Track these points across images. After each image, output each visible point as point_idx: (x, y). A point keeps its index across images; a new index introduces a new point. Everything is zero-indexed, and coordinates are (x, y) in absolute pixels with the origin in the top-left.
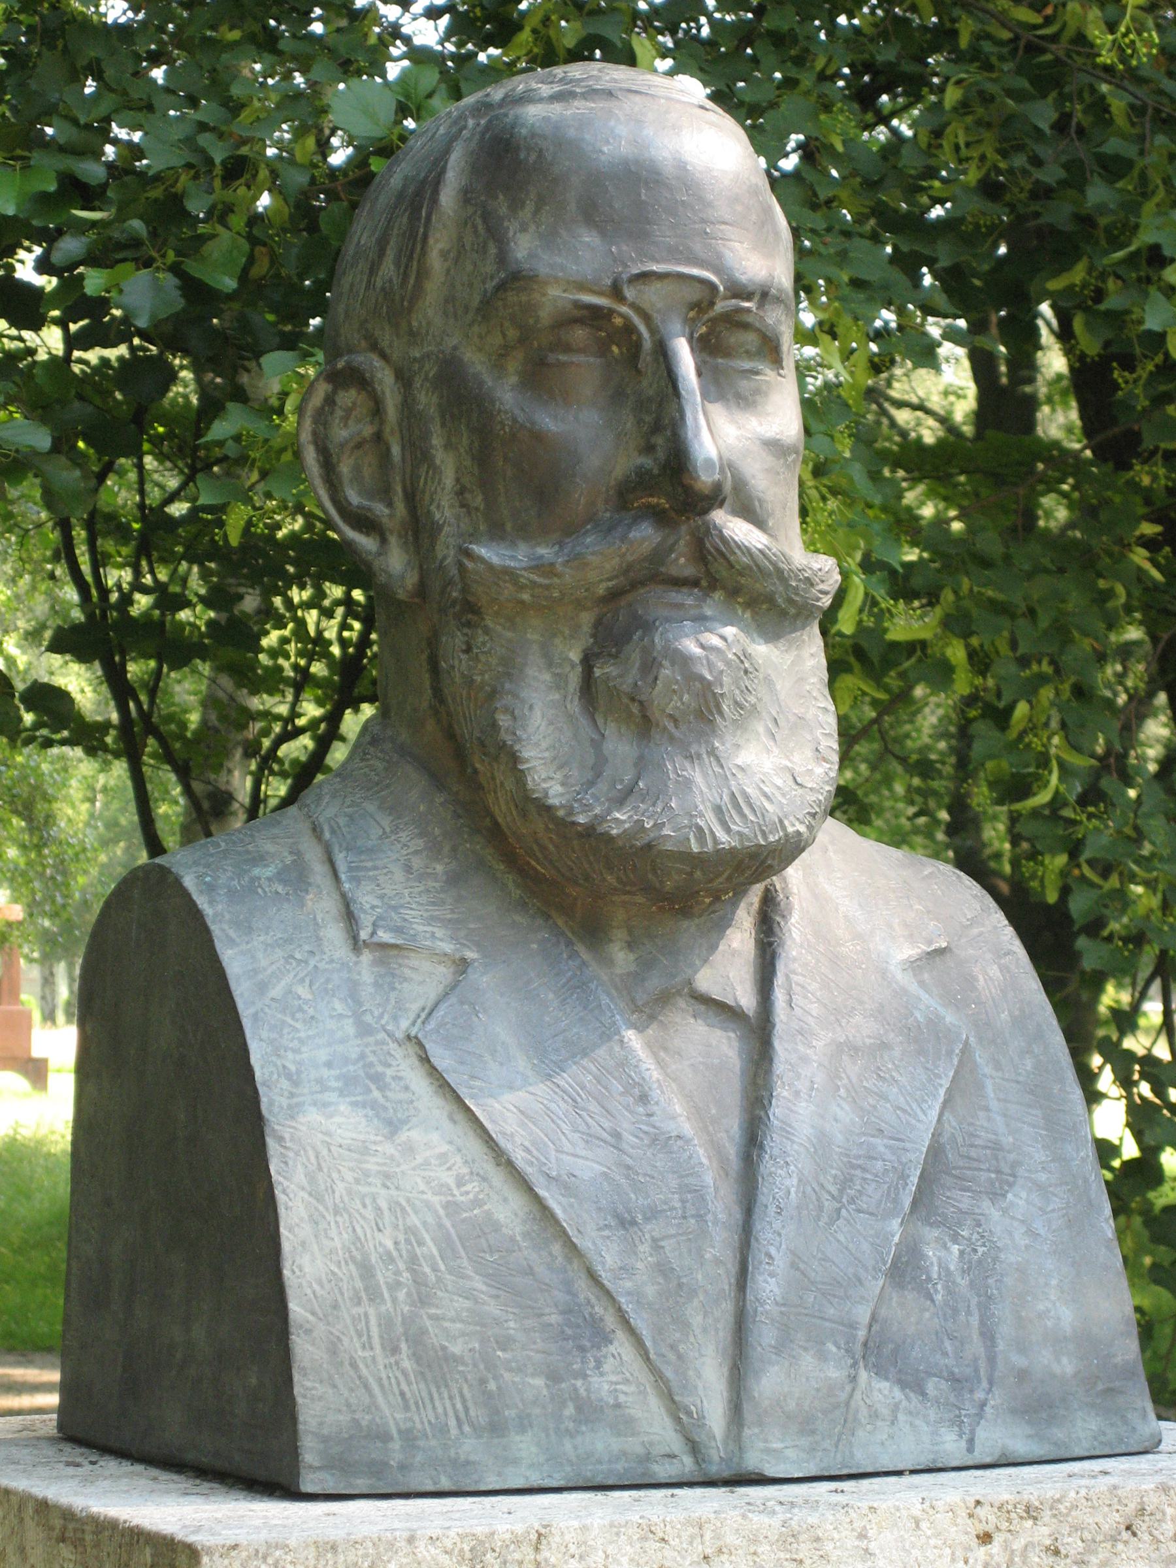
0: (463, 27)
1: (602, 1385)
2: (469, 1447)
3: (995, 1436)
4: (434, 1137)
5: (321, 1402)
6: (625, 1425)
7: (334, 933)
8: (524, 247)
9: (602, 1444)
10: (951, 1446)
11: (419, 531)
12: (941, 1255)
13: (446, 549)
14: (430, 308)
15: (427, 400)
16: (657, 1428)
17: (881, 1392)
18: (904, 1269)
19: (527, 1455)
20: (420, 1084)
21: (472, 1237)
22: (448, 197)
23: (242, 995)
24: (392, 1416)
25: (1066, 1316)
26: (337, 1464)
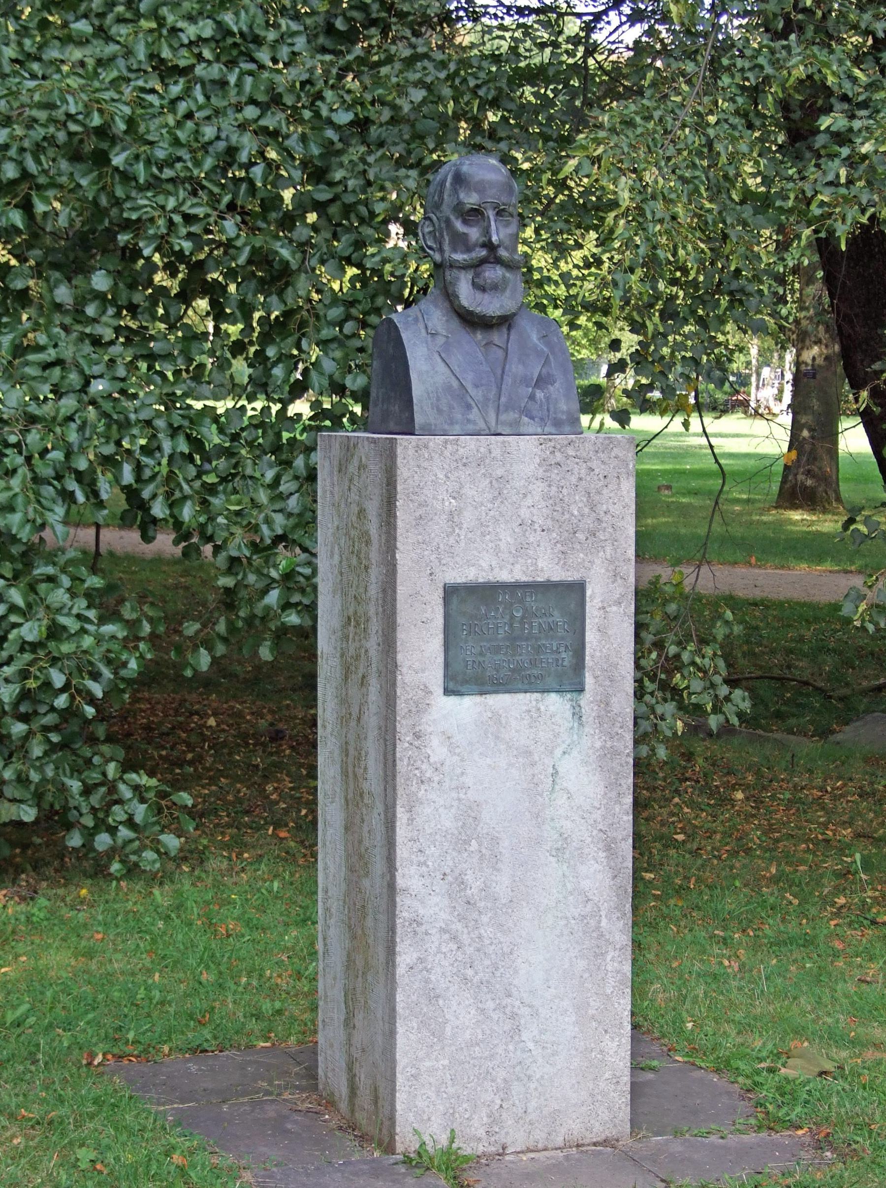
0: (781, 28)
1: (471, 417)
2: (446, 427)
3: (547, 429)
4: (441, 367)
5: (419, 419)
6: (475, 423)
7: (423, 331)
8: (462, 195)
9: (470, 427)
10: (539, 430)
11: (441, 250)
12: (539, 395)
13: (447, 255)
14: (444, 207)
15: (443, 225)
16: (482, 425)
17: (526, 419)
18: (532, 397)
19: (457, 428)
20: (439, 360)
21: (448, 388)
22: (448, 184)
23: (621, 1035)
24: (433, 422)
25: (565, 408)
26: (421, 429)
